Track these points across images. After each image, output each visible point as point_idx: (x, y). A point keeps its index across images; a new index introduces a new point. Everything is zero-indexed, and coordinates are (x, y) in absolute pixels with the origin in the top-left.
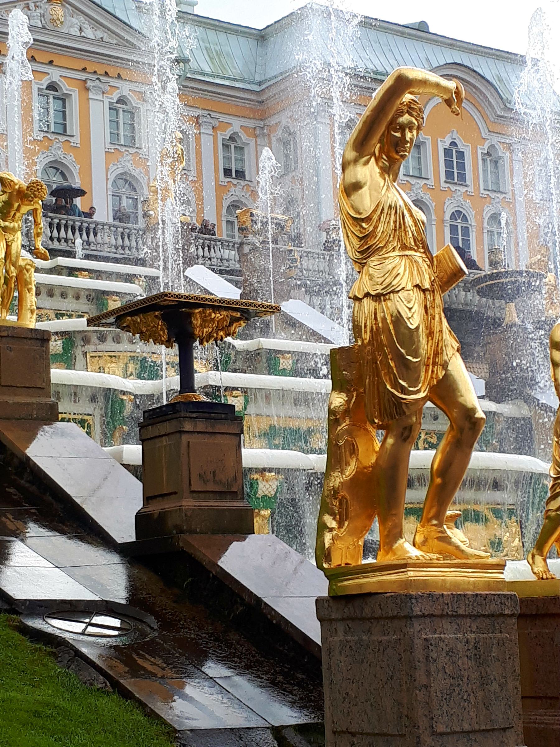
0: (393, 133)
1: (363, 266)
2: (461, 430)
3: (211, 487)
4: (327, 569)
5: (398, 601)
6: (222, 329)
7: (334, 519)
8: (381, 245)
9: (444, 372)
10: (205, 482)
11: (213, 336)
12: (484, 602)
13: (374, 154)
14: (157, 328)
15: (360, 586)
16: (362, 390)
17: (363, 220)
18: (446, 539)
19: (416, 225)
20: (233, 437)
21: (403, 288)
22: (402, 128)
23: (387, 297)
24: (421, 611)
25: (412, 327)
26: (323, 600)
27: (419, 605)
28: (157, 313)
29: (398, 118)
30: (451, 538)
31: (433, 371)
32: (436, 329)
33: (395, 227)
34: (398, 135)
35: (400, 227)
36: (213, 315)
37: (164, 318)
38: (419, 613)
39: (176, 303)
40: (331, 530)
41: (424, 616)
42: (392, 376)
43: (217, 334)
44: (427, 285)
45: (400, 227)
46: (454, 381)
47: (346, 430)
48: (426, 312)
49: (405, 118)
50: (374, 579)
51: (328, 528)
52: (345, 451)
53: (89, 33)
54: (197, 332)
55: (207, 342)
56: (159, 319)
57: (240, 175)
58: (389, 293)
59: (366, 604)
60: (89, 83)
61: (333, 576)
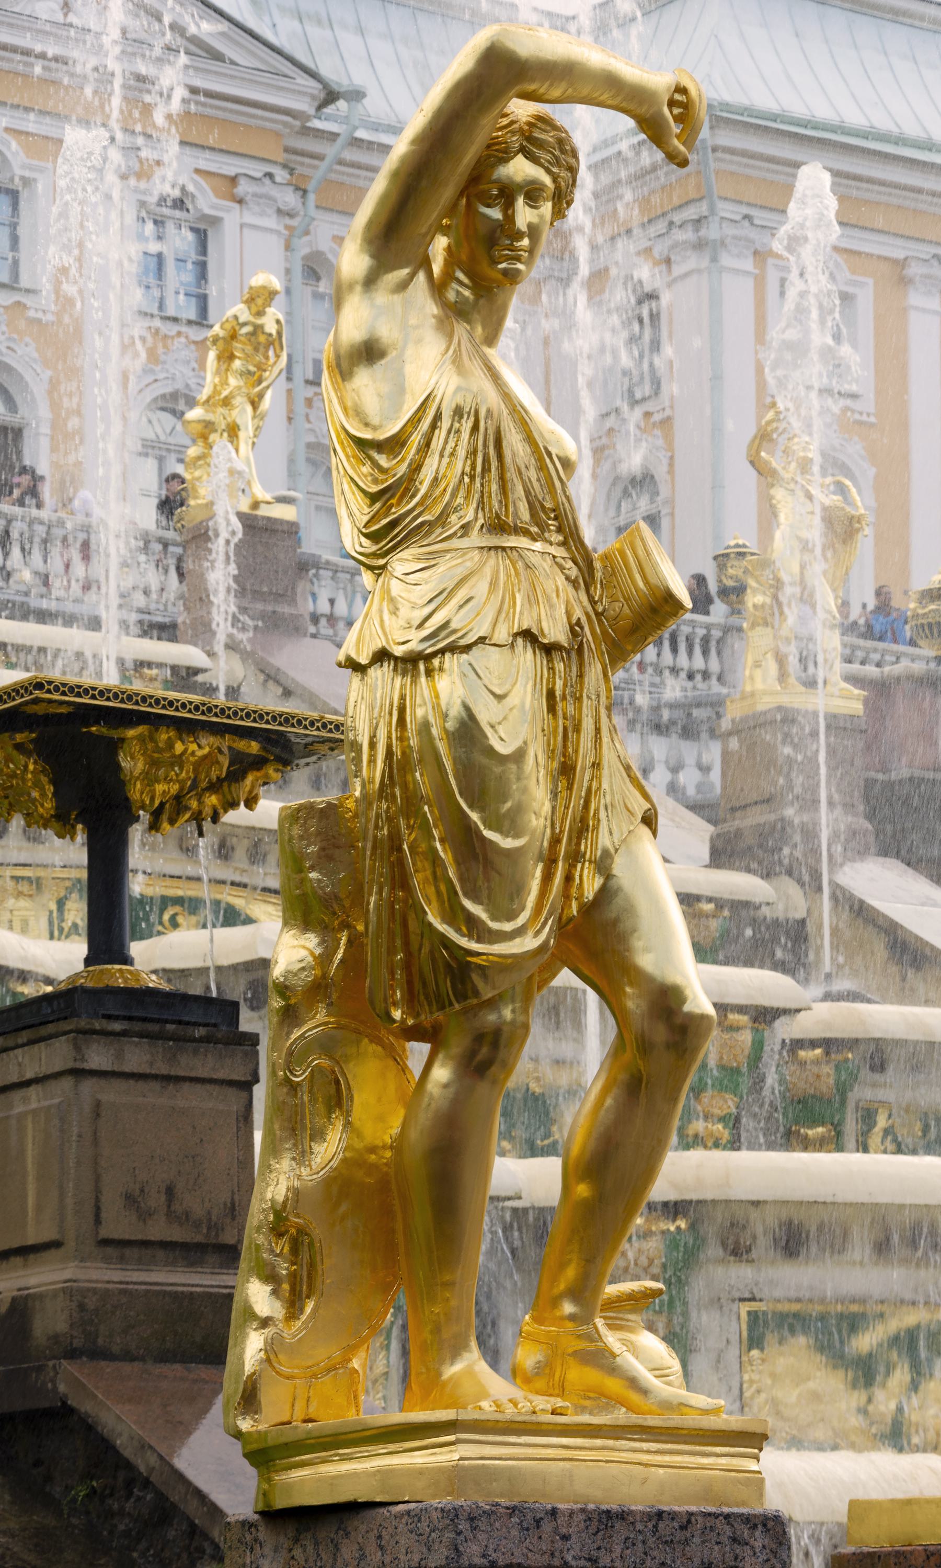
2: (644, 1047)
3: (158, 1230)
4: (249, 1433)
5: (424, 1526)
6: (214, 787)
8: (427, 517)
9: (598, 882)
10: (145, 1215)
11: (187, 808)
12: (679, 1535)
13: (426, 263)
14: (24, 780)
17: (379, 446)
18: (601, 1359)
19: (542, 467)
20: (231, 1092)
21: (482, 640)
22: (507, 194)
23: (436, 662)
25: (503, 749)
28: (19, 737)
29: (494, 166)
30: (614, 1356)
31: (568, 878)
32: (584, 758)
33: (473, 467)
34: (495, 214)
35: (486, 469)
36: (179, 747)
39: (71, 709)
42: (443, 888)
43: (200, 802)
44: (556, 632)
45: (486, 469)
46: (630, 909)
47: (316, 1038)
48: (552, 709)
49: (520, 168)
52: (313, 1100)
54: (136, 792)
55: (172, 822)
56: (28, 754)
58: (442, 651)
59: (347, 1535)
60: (244, 187)
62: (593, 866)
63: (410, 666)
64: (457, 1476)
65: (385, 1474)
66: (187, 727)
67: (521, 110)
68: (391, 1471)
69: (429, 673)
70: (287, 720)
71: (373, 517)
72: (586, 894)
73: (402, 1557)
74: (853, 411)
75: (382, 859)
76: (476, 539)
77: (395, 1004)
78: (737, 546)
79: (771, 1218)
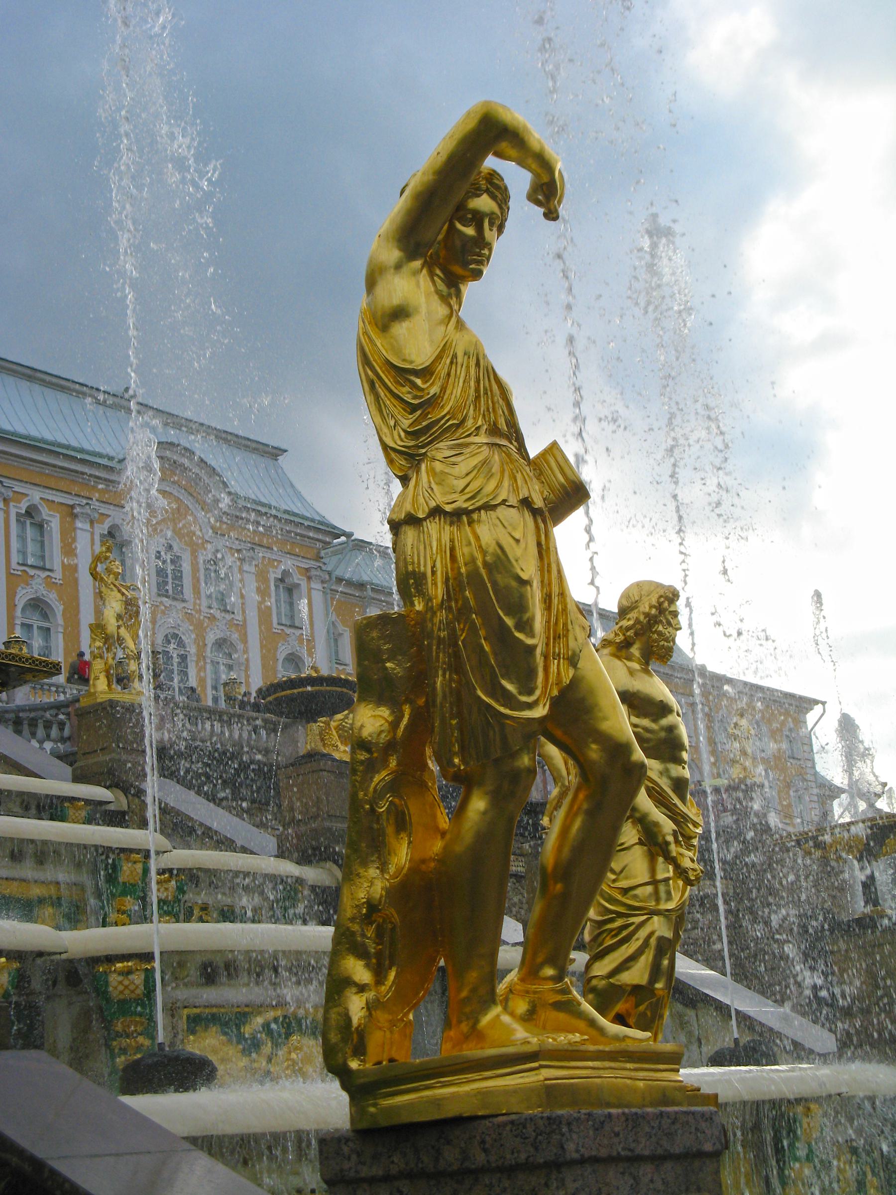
0: (459, 226)
1: (420, 462)
4: (358, 1071)
7: (367, 966)
9: (571, 672)
15: (437, 1102)
16: (421, 701)
23: (475, 516)
24: (577, 1151)
26: (339, 1140)
27: (575, 1136)
34: (470, 231)
38: (576, 1156)
40: (362, 989)
41: (582, 1161)
45: (486, 393)
49: (484, 203)
50: (467, 1088)
51: (356, 984)
58: (479, 509)
61: (359, 1089)
62: (566, 662)
63: (455, 519)
64: (550, 1093)
65: (484, 1094)
68: (490, 1092)
69: (470, 523)
70: (13, 658)
71: (415, 421)
72: (564, 680)
73: (508, 1156)
74: (52, 578)
75: (444, 652)
76: (482, 439)
77: (455, 754)
78: (15, 637)
79: (199, 959)
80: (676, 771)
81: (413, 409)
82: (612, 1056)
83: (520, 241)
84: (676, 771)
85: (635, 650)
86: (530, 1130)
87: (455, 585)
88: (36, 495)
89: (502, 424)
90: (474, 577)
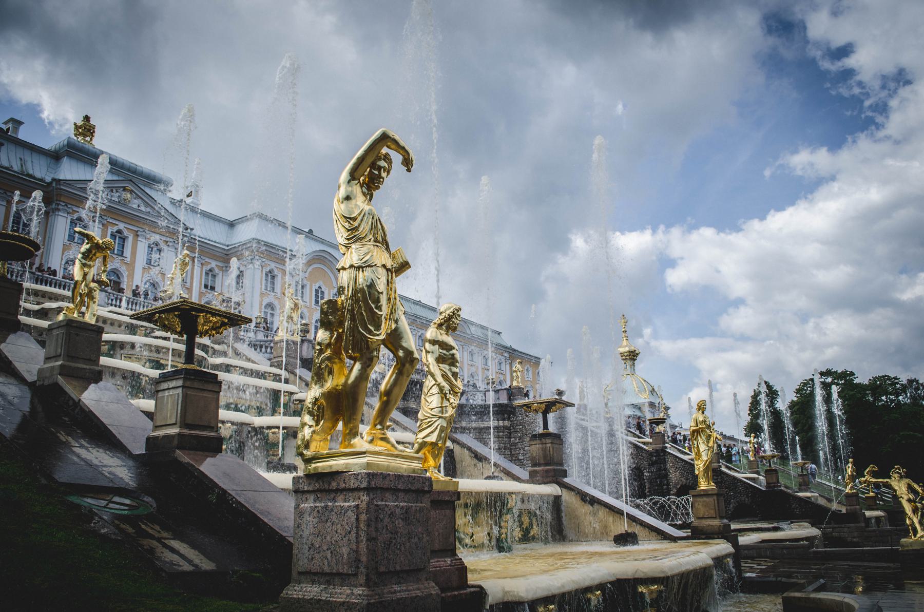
6: (215, 329)
15: (331, 467)
16: (341, 331)
17: (350, 218)
34: (376, 172)
37: (179, 316)
44: (389, 266)
49: (382, 163)
53: (143, 208)
54: (200, 328)
57: (213, 288)
66: (213, 315)
67: (384, 150)
80: (454, 369)
81: (349, 230)
82: (397, 456)
83: (395, 178)
84: (454, 369)
85: (444, 327)
86: (359, 477)
87: (356, 291)
88: (121, 226)
89: (380, 239)
90: (362, 290)
